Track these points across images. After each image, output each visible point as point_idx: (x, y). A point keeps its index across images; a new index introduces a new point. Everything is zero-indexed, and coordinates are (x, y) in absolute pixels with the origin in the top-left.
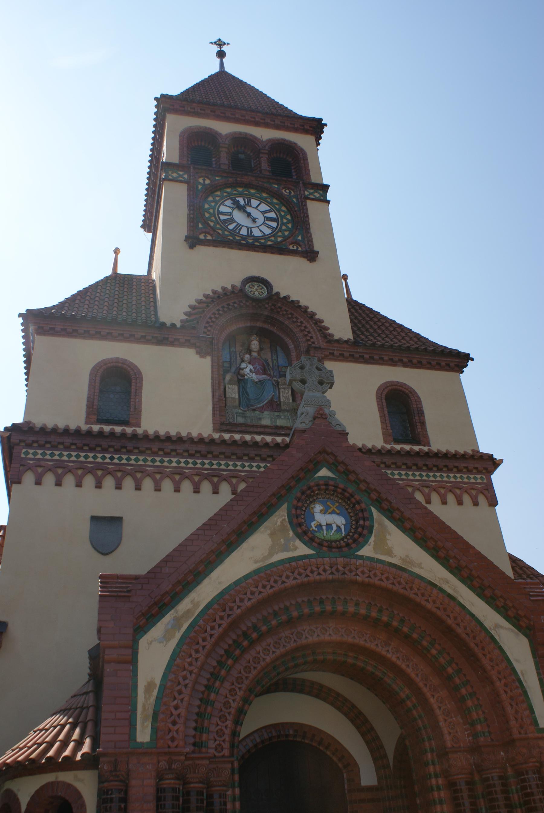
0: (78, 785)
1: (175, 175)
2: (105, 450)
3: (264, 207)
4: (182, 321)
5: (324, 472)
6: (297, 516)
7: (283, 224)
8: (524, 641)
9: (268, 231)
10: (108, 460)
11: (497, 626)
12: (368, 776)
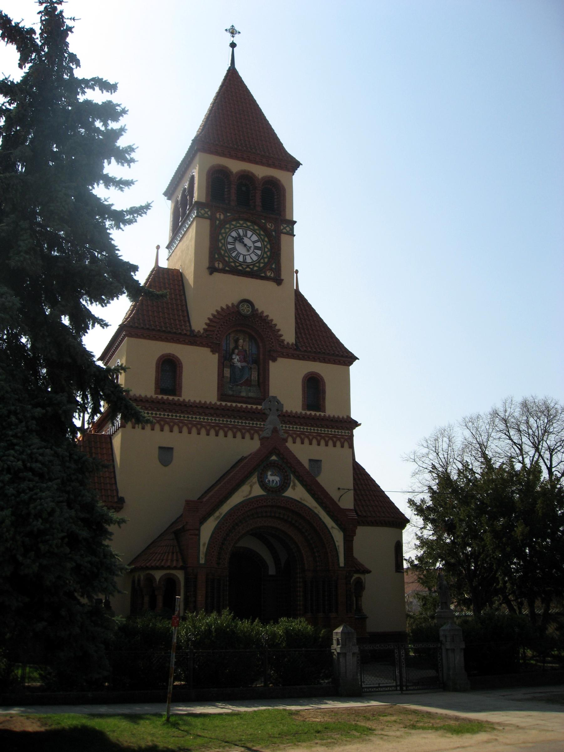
0: (178, 576)
1: (203, 212)
2: (165, 410)
3: (255, 238)
4: (204, 329)
5: (274, 458)
6: (261, 478)
7: (265, 252)
8: (342, 534)
9: (255, 258)
10: (166, 416)
11: (333, 527)
12: (272, 571)
